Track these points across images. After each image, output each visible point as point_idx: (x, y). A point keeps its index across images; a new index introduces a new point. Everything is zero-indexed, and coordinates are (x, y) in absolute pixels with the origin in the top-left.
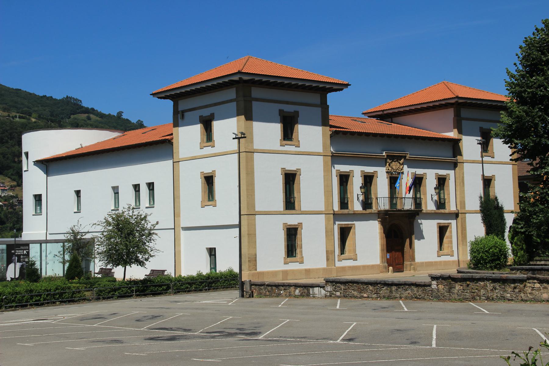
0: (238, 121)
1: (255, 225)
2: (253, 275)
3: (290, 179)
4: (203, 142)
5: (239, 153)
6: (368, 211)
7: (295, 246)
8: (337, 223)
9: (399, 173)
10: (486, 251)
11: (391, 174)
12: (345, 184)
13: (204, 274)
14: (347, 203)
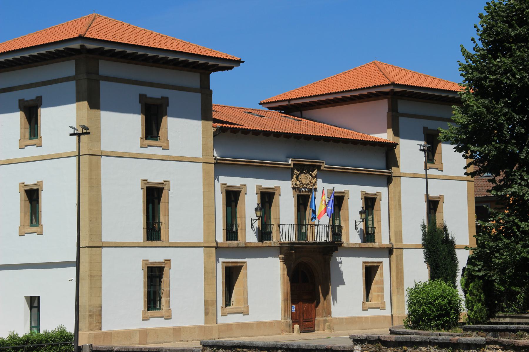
0: (78, 109)
1: (101, 262)
2: (96, 337)
3: (154, 195)
4: (25, 139)
5: (79, 156)
6: (266, 243)
7: (160, 294)
8: (221, 260)
9: (310, 190)
10: (430, 303)
12: (233, 204)
13: (21, 335)
14: (236, 232)
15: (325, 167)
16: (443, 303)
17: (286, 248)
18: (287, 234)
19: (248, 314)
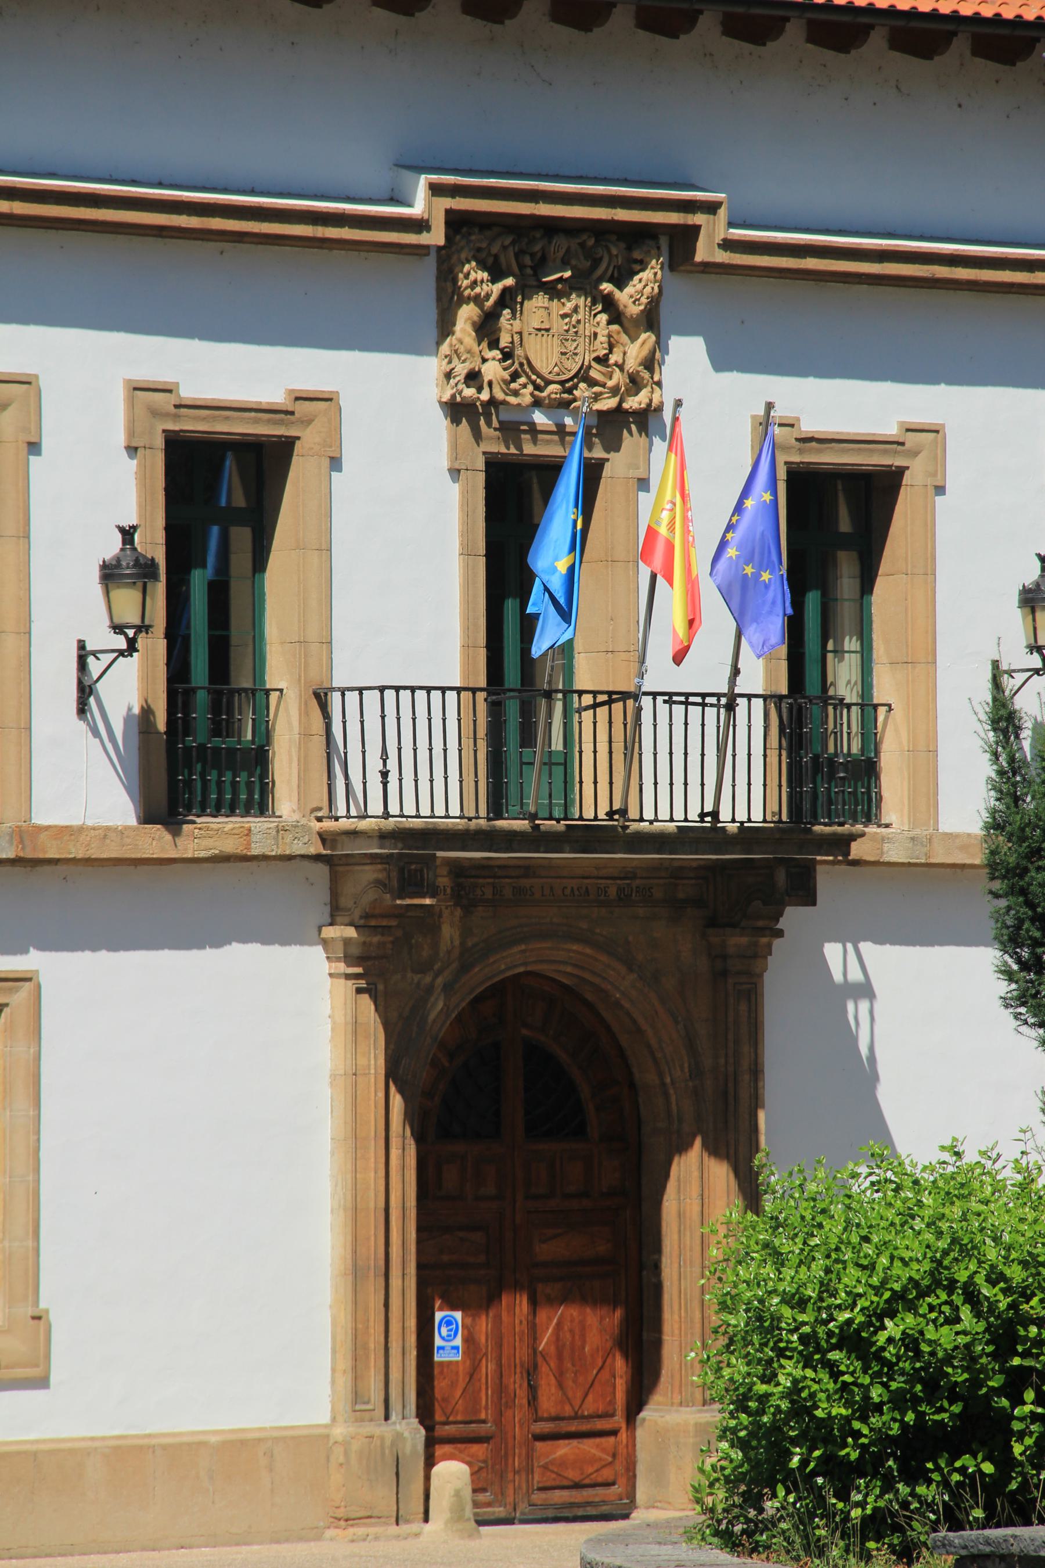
6: (210, 834)
9: (611, 426)
10: (852, 1340)
11: (510, 430)
15: (728, 245)
16: (946, 1337)
17: (369, 874)
18: (375, 764)
19: (42, 1382)
